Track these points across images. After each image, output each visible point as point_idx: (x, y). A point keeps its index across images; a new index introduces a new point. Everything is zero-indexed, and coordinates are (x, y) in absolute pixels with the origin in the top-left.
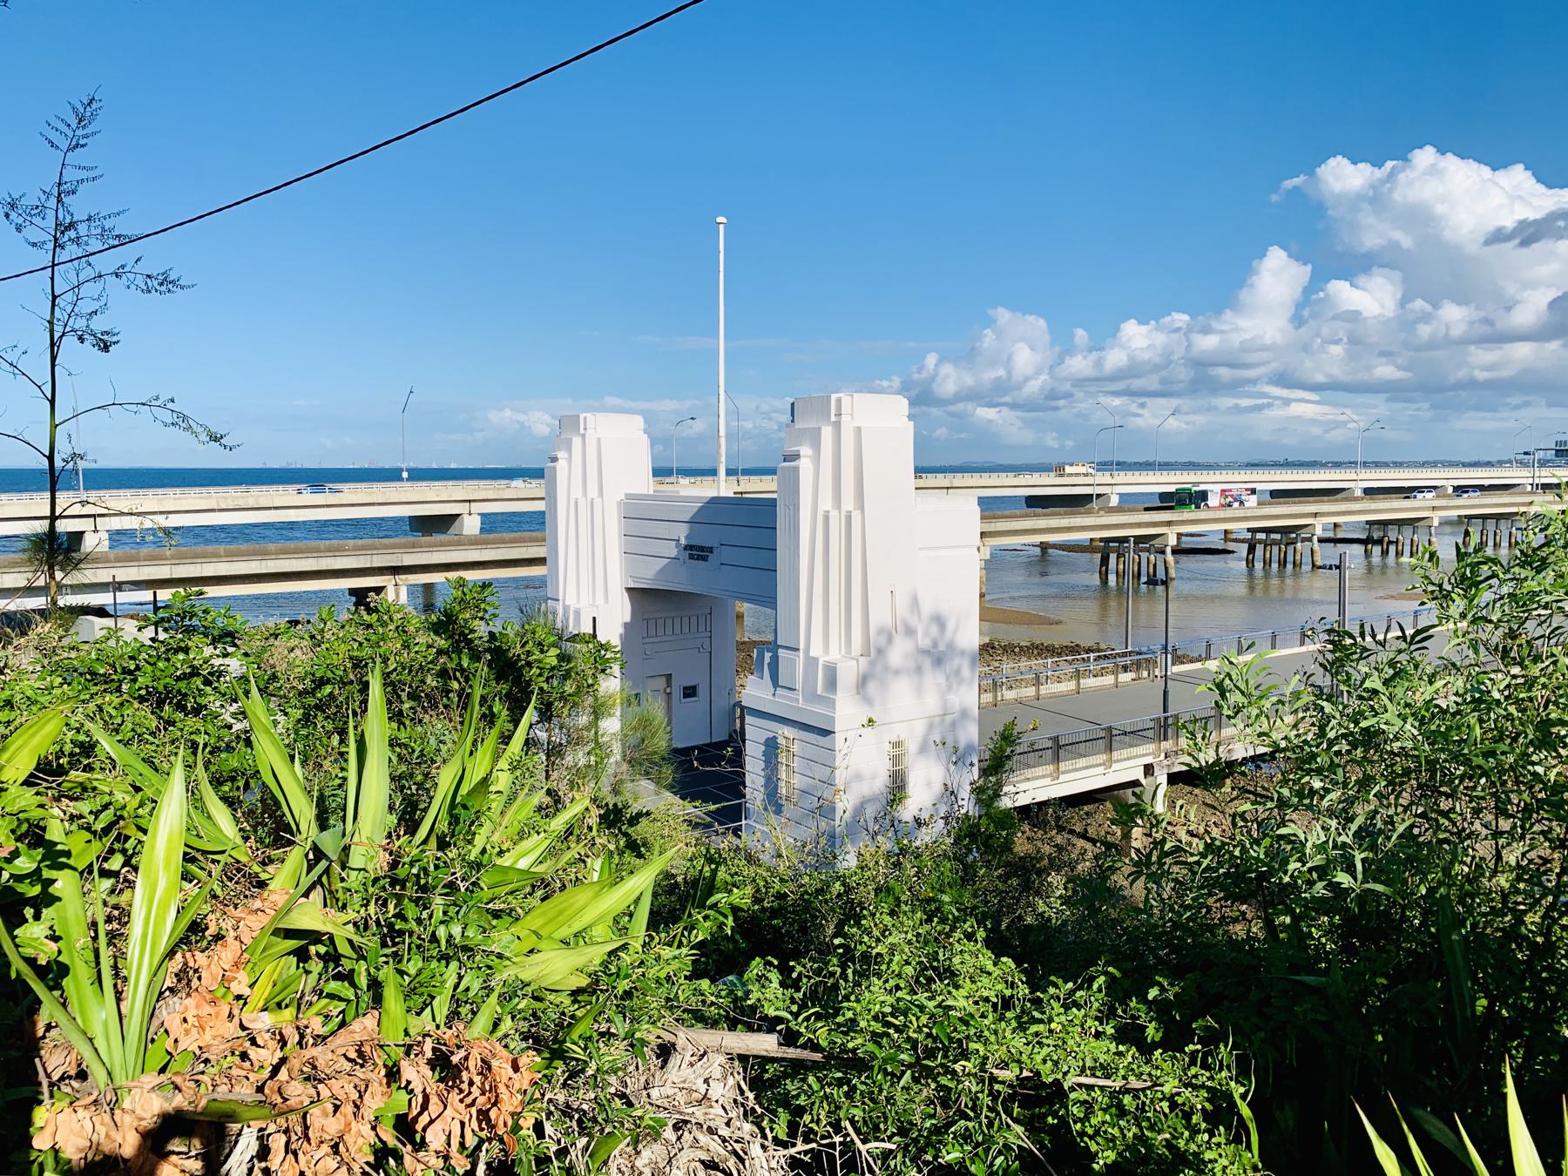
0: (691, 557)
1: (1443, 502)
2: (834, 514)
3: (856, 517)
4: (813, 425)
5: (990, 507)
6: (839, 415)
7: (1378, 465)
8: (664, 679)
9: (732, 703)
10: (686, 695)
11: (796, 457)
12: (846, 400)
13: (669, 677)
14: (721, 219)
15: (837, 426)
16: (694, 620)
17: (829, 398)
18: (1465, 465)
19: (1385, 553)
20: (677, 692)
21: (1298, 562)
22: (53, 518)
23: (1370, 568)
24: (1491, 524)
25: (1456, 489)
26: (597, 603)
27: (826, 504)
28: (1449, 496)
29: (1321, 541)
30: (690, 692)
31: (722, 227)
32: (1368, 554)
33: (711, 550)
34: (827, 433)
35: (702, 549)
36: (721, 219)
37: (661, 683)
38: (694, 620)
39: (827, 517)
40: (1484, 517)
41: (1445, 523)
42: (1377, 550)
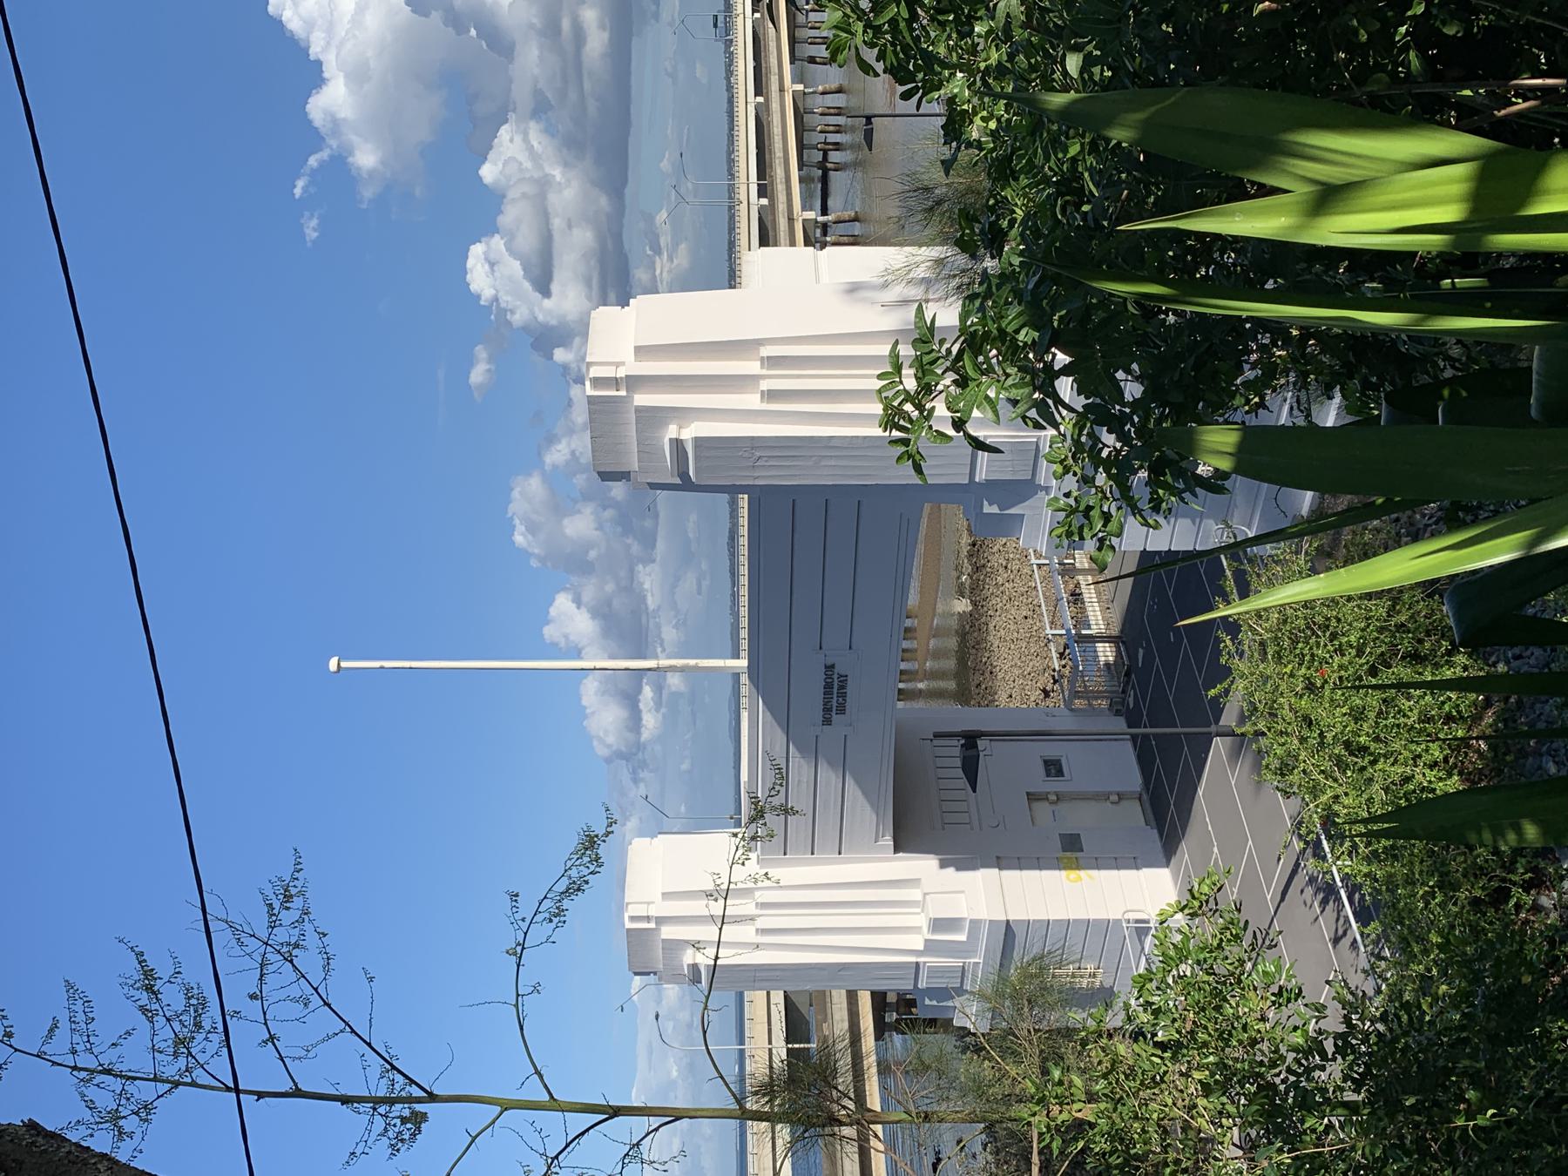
0: (842, 710)
1: (782, 207)
2: (765, 385)
3: (766, 351)
4: (633, 416)
5: (766, 238)
6: (648, 919)
7: (731, 163)
8: (1037, 806)
9: (1067, 712)
10: (1060, 773)
11: (678, 444)
12: (633, 910)
13: (1032, 797)
14: (333, 664)
15: (661, 921)
16: (940, 762)
17: (628, 930)
18: (731, 129)
19: (837, 146)
20: (1053, 786)
21: (851, 239)
22: (717, 958)
23: (856, 164)
24: (803, 33)
25: (758, 93)
26: (919, 897)
27: (752, 401)
28: (767, 100)
29: (824, 212)
30: (1053, 768)
31: (343, 664)
32: (839, 168)
33: (830, 668)
34: (668, 932)
35: (828, 687)
36: (333, 664)
37: (1042, 809)
38: (940, 762)
39: (771, 395)
40: (793, 41)
41: (799, 78)
42: (835, 157)
